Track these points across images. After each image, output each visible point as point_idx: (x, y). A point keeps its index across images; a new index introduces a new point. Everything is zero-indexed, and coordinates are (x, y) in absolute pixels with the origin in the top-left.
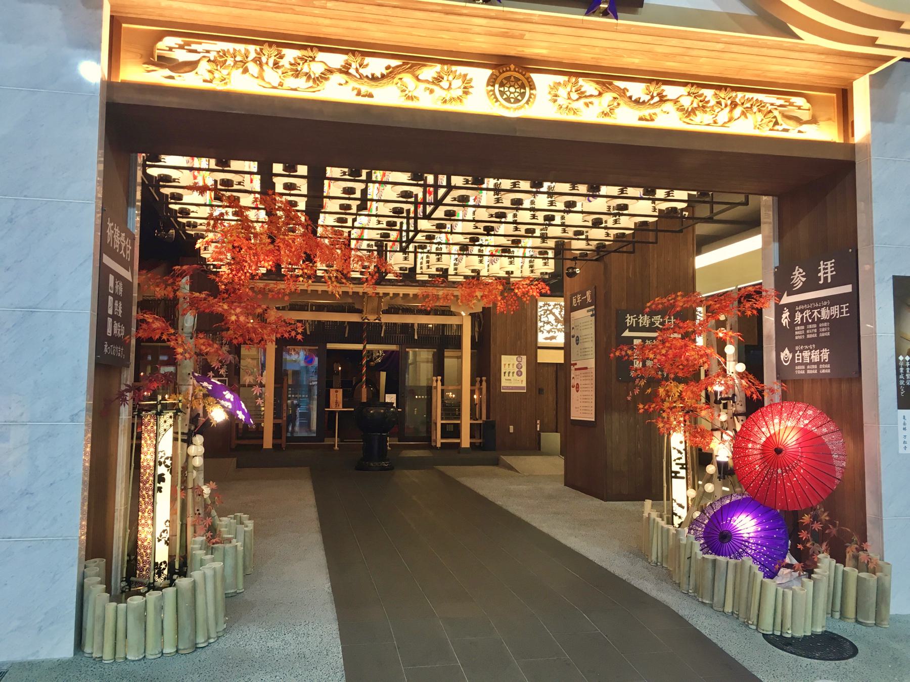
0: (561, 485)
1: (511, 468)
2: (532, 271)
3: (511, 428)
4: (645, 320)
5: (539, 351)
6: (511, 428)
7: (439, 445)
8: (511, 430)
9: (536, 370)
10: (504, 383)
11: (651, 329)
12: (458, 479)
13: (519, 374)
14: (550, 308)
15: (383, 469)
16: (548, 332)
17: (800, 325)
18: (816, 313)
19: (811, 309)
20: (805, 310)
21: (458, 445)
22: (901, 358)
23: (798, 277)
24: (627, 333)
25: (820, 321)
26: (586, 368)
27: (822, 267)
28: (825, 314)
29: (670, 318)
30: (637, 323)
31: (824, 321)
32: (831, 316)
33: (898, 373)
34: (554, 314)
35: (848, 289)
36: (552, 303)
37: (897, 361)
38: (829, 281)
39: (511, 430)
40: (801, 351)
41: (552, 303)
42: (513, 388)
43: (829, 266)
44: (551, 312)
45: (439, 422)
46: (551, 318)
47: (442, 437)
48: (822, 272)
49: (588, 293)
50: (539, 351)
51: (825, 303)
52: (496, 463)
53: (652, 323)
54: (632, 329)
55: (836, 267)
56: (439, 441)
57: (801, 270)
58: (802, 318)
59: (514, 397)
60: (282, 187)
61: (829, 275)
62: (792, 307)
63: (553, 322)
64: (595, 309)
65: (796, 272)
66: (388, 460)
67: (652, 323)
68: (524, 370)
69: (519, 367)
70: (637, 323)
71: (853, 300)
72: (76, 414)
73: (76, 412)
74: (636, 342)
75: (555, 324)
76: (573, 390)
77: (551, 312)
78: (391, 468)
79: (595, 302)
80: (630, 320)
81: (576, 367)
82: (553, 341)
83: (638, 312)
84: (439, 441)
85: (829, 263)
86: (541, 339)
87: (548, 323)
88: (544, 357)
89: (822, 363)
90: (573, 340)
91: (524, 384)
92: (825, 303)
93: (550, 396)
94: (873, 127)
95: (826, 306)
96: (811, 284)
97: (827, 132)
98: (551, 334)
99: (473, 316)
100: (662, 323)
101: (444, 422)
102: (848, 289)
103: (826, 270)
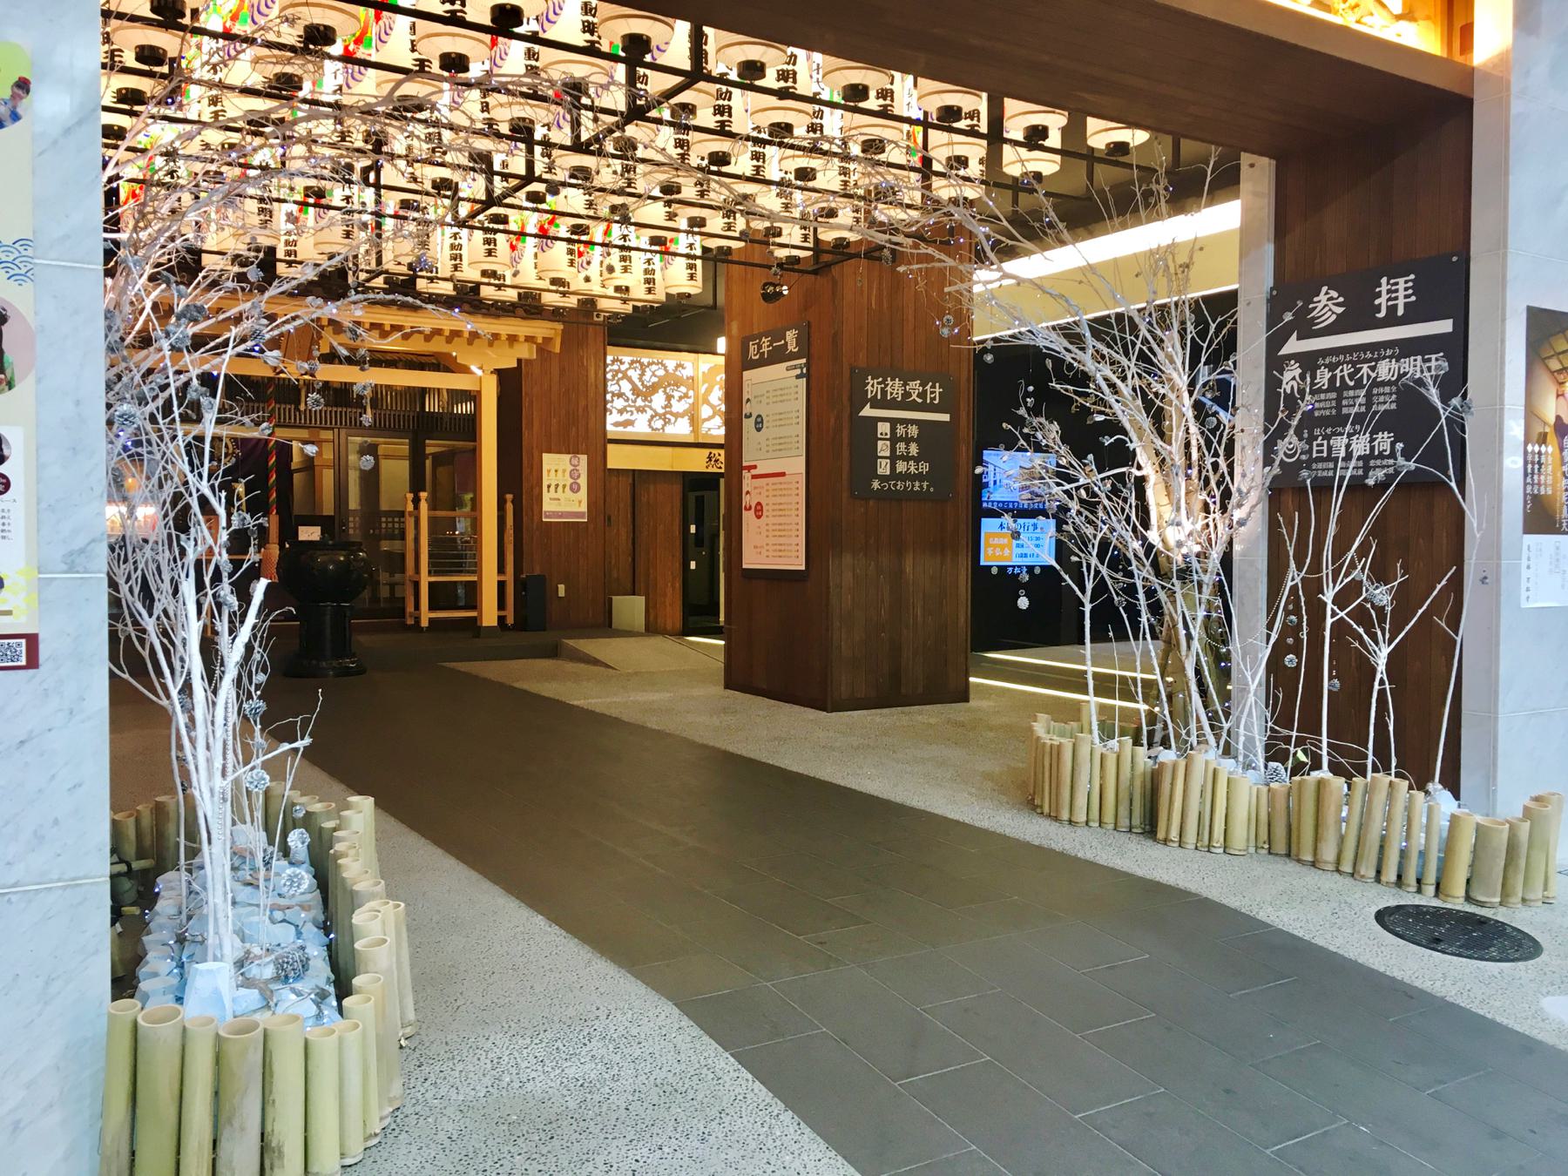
0: (718, 690)
1: (596, 662)
2: (650, 291)
3: (562, 588)
4: (895, 388)
5: (610, 447)
6: (562, 588)
7: (425, 623)
8: (562, 593)
9: (603, 480)
10: (548, 505)
11: (905, 404)
12: (517, 685)
13: (575, 488)
14: (623, 368)
15: (347, 672)
16: (621, 412)
17: (1326, 391)
18: (1365, 369)
19: (1354, 364)
20: (1339, 364)
21: (473, 625)
22: (1530, 448)
23: (1327, 305)
24: (867, 411)
25: (1376, 383)
26: (783, 474)
27: (1384, 288)
28: (1385, 370)
29: (933, 386)
30: (884, 392)
31: (1383, 384)
32: (1401, 376)
33: (1526, 475)
34: (630, 380)
35: (1445, 326)
36: (627, 359)
37: (1526, 452)
38: (1400, 312)
39: (562, 593)
40: (1327, 437)
41: (627, 359)
42: (562, 515)
43: (1401, 286)
44: (626, 377)
45: (425, 580)
46: (626, 387)
47: (431, 608)
48: (1385, 296)
49: (791, 336)
50: (610, 447)
51: (1389, 352)
52: (554, 652)
53: (907, 394)
54: (876, 404)
55: (1417, 288)
56: (426, 616)
57: (1334, 294)
58: (1332, 380)
59: (568, 530)
60: (133, 55)
61: (1401, 303)
62: (1309, 362)
63: (629, 394)
64: (808, 365)
65: (1322, 297)
66: (354, 655)
67: (907, 394)
68: (583, 481)
69: (574, 474)
70: (884, 392)
71: (1456, 348)
72: (82, 551)
73: (80, 542)
74: (884, 428)
75: (632, 397)
76: (748, 517)
77: (626, 377)
78: (360, 671)
79: (806, 348)
80: (873, 387)
81: (754, 472)
82: (630, 429)
83: (884, 373)
84: (426, 616)
85: (1401, 280)
86: (612, 423)
87: (620, 395)
88: (618, 458)
89: (1376, 458)
90: (748, 425)
91: (584, 508)
92: (1389, 352)
93: (621, 534)
94: (1515, 37)
95: (1391, 357)
96: (1359, 315)
97: (1424, 37)
98: (626, 416)
99: (501, 373)
100: (922, 395)
101: (433, 579)
102: (1445, 326)
103: (1396, 292)
